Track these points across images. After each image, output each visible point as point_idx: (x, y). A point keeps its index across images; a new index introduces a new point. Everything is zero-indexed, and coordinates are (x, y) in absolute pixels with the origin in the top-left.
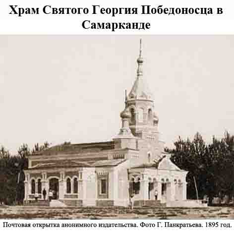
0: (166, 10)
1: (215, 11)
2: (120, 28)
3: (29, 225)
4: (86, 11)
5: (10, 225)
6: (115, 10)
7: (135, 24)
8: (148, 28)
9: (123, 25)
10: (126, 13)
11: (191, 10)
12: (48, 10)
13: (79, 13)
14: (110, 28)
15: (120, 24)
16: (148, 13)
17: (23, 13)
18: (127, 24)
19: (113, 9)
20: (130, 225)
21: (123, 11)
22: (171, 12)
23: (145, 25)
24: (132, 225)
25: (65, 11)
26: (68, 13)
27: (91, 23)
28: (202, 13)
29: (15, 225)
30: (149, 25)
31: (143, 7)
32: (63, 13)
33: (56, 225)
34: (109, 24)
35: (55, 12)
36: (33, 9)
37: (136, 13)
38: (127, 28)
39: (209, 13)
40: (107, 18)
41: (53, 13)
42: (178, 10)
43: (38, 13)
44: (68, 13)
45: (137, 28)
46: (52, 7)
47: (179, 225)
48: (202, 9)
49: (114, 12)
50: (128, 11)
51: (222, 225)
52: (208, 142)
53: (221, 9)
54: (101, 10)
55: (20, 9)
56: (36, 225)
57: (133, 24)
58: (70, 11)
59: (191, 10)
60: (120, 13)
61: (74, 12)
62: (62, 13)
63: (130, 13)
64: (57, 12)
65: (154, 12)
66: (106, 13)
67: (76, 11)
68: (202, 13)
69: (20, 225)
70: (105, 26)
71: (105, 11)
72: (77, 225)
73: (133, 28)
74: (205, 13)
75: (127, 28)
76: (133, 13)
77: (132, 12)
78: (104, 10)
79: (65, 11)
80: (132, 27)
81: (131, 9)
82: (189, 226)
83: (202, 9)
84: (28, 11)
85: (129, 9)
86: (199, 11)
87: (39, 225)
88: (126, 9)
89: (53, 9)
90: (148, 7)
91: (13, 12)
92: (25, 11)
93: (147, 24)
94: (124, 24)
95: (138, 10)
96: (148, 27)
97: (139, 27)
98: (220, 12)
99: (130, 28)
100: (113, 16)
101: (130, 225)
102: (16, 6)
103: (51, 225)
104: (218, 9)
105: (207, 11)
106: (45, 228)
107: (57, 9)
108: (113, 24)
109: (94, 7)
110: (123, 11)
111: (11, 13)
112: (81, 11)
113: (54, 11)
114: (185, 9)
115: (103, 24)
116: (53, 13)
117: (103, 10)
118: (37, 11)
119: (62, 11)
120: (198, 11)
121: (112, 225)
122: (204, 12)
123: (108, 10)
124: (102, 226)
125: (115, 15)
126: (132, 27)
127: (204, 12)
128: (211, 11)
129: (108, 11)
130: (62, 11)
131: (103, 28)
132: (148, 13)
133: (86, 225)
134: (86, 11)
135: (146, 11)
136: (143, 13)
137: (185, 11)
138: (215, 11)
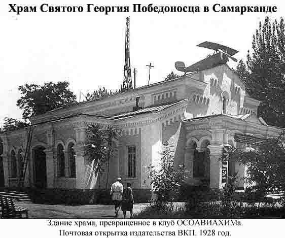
1: (202, 9)
2: (248, 11)
3: (91, 234)
5: (67, 234)
11: (180, 9)
12: (45, 8)
13: (74, 11)
14: (239, 11)
15: (248, 7)
16: (139, 11)
17: (22, 11)
18: (255, 8)
19: (106, 8)
21: (116, 9)
22: (161, 10)
23: (272, 8)
24: (170, 234)
25: (61, 9)
26: (64, 11)
27: (221, 6)
28: (189, 11)
29: (74, 234)
30: (276, 8)
31: (135, 5)
32: (59, 11)
35: (52, 10)
36: (229, 8)
37: (128, 11)
38: (255, 11)
39: (196, 11)
41: (50, 11)
43: (35, 11)
44: (64, 11)
45: (264, 11)
46: (49, 6)
47: (106, 234)
48: (189, 7)
53: (208, 8)
54: (95, 9)
55: (18, 7)
57: (261, 7)
58: (66, 9)
59: (180, 9)
63: (121, 11)
64: (53, 11)
65: (144, 10)
66: (99, 11)
67: (263, 9)
68: (189, 11)
69: (79, 233)
70: (234, 9)
73: (261, 11)
77: (123, 10)
78: (98, 8)
79: (61, 9)
80: (259, 10)
81: (123, 8)
82: (120, 234)
83: (189, 7)
84: (26, 10)
85: (121, 7)
86: (187, 9)
89: (50, 7)
90: (139, 5)
91: (12, 10)
92: (24, 9)
94: (252, 7)
95: (87, 10)
96: (275, 10)
97: (266, 11)
99: (258, 11)
100: (106, 14)
102: (15, 5)
103: (117, 234)
104: (205, 7)
105: (194, 9)
107: (53, 8)
108: (242, 7)
109: (89, 5)
110: (116, 9)
112: (76, 9)
115: (233, 8)
118: (81, 9)
119: (58, 9)
121: (146, 234)
122: (191, 10)
123: (102, 8)
124: (135, 234)
126: (259, 10)
127: (191, 10)
128: (198, 10)
130: (58, 9)
131: (233, 11)
132: (139, 11)
133: (158, 234)
135: (137, 9)
136: (135, 11)
137: (173, 9)
138: (202, 9)
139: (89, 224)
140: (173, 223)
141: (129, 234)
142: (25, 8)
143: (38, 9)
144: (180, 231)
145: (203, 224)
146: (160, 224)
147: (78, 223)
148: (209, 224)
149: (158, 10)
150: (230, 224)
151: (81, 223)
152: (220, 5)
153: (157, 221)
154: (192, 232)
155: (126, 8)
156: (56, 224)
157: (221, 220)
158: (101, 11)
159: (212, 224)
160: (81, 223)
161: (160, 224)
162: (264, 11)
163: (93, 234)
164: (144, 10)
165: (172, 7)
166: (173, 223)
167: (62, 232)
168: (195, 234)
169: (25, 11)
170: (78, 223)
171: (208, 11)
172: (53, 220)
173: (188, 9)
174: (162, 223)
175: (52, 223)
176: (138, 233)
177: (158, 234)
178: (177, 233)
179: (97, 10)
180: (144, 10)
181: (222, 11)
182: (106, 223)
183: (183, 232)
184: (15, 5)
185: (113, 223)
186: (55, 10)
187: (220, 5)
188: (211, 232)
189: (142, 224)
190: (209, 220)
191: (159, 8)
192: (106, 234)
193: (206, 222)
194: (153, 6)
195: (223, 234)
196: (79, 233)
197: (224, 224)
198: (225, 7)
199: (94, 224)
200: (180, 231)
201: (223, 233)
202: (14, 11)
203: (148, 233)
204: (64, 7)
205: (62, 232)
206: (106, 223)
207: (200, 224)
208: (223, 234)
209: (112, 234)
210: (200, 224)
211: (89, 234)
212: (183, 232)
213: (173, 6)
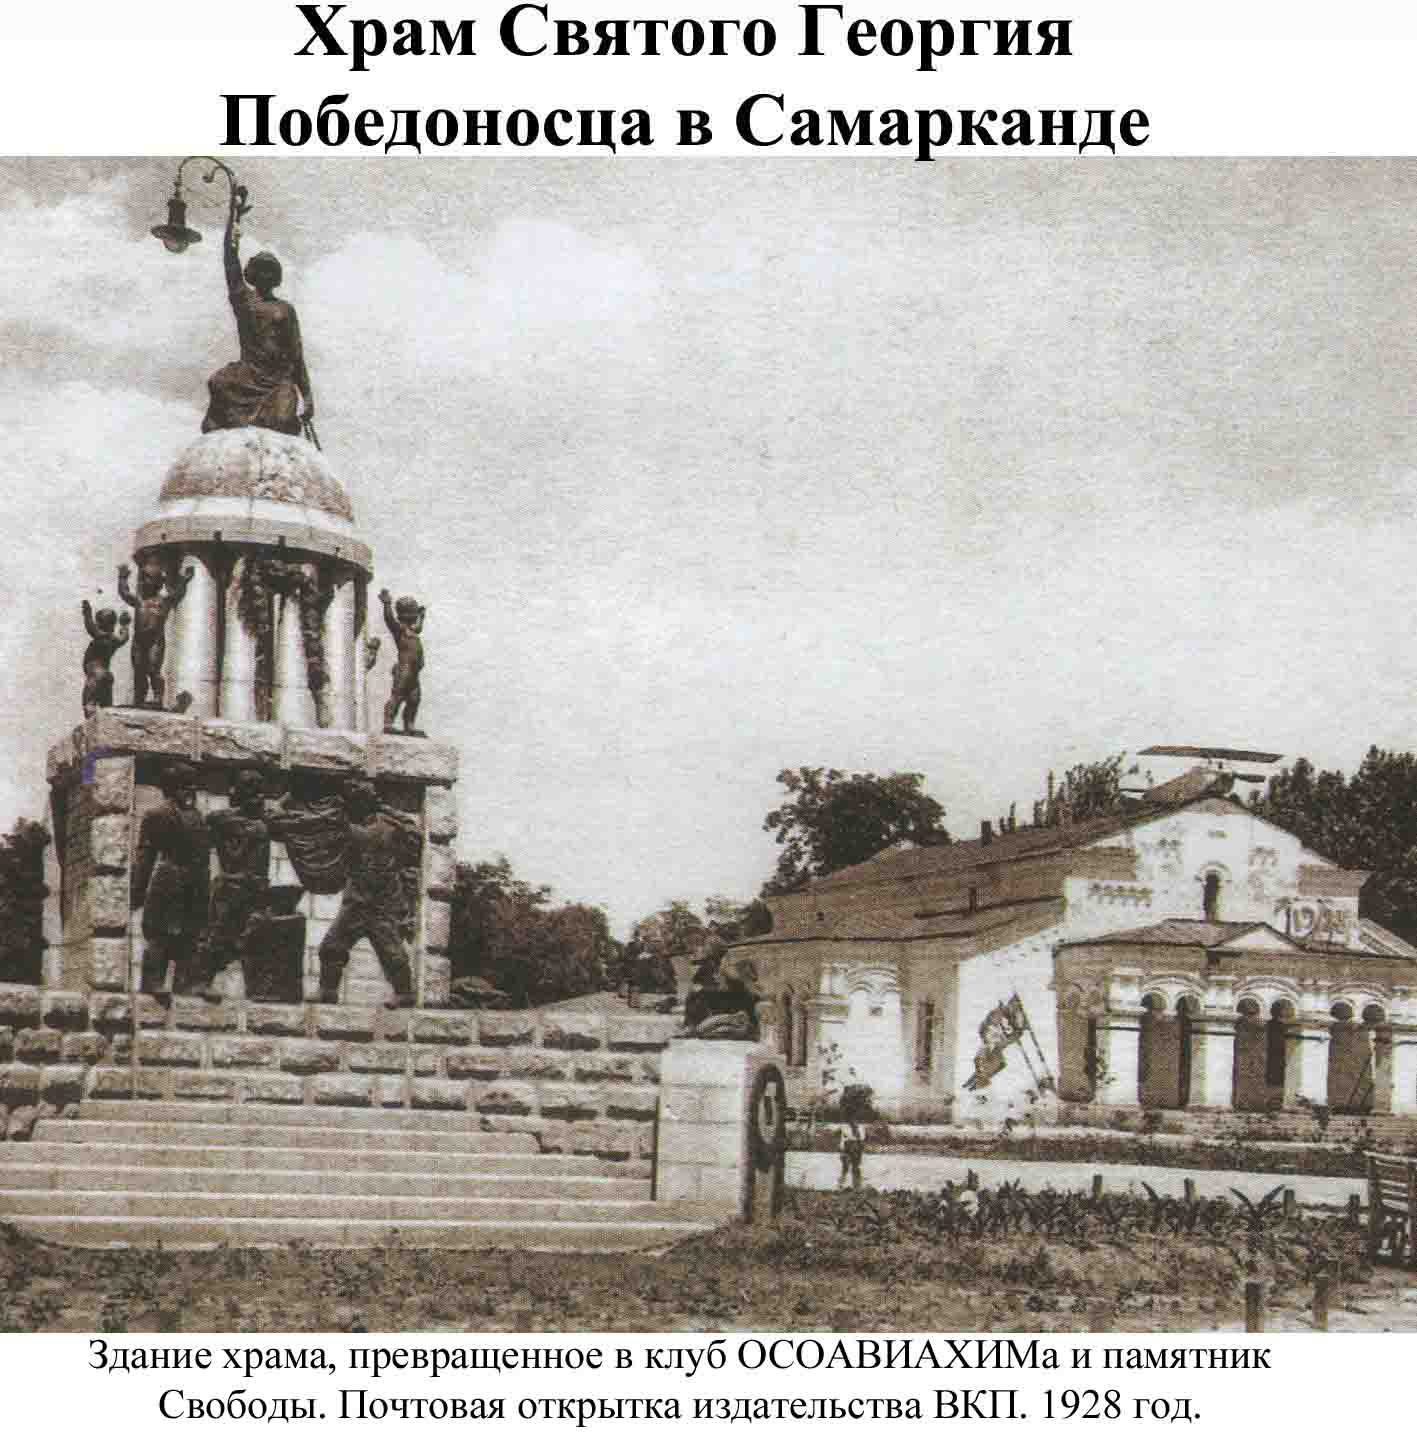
0: (370, 119)
1: (666, 129)
2: (967, 140)
3: (498, 1410)
4: (760, 38)
5: (378, 1409)
6: (937, 34)
7: (1058, 120)
8: (1130, 140)
9: (987, 124)
10: (1003, 49)
13: (718, 49)
14: (904, 139)
15: (967, 116)
18: (1007, 118)
19: (926, 27)
20: (882, 1409)
21: (985, 39)
22: (402, 136)
24: (894, 1408)
25: (636, 39)
26: (651, 48)
27: (791, 108)
29: (412, 1409)
30: (1144, 122)
32: (621, 50)
33: (661, 1408)
34: (1025, 117)
35: (573, 45)
37: (1064, 50)
38: (1008, 139)
39: (627, 139)
40: (891, 83)
41: (563, 49)
42: (442, 132)
43: (467, 50)
44: (651, 48)
45: (1068, 139)
46: (555, 14)
47: (574, 1408)
48: (586, 117)
49: (929, 42)
50: (1012, 38)
51: (1146, 1408)
52: (554, 904)
53: (704, 117)
54: (855, 26)
55: (359, 27)
56: (541, 1408)
57: (1047, 116)
58: (664, 38)
60: (969, 49)
61: (688, 45)
62: (613, 47)
63: (1023, 50)
64: (584, 46)
66: (880, 48)
69: (439, 1409)
70: (876, 128)
71: (877, 40)
72: (756, 1410)
74: (606, 139)
75: (1008, 139)
76: (1046, 50)
77: (1036, 42)
78: (871, 31)
79: (636, 39)
80: (1036, 131)
81: (1033, 30)
82: (641, 1409)
83: (586, 117)
85: (1023, 27)
86: (570, 130)
87: (554, 1409)
88: (1003, 26)
89: (563, 26)
90: (263, 103)
91: (319, 46)
92: (392, 38)
93: (1127, 116)
94: (992, 115)
96: (1137, 133)
98: (696, 135)
100: (926, 65)
101: (882, 1409)
102: (336, 8)
103: (627, 1410)
104: (685, 116)
105: (618, 128)
106: (594, 1423)
107: (582, 28)
108: (924, 117)
109: (811, 13)
110: (985, 39)
111: (304, 52)
112: (733, 38)
113: (569, 38)
114: (482, 120)
115: (864, 117)
116: (563, 49)
117: (862, 29)
120: (562, 129)
121: (773, 1409)
124: (716, 1409)
125: (935, 59)
126: (1036, 131)
129: (894, 37)
132: (262, 138)
133: (831, 1409)
134: (760, 38)
138: (666, 129)
139: (299, 1360)
140: (717, 1358)
141: (688, 1409)
142: (399, 29)
143: (487, 36)
144: (947, 1398)
145: (869, 1360)
146: (652, 1360)
147: (241, 1358)
148: (900, 1361)
149: (386, 131)
150: (1004, 1361)
151: (254, 1357)
152: (780, 101)
153: (638, 1343)
154: (1003, 1401)
155: (1054, 30)
156: (141, 1361)
157: (959, 1338)
158: (890, 51)
159: (913, 1362)
160: (254, 1357)
161: (652, 1360)
162: (1068, 139)
163: (510, 1409)
164: (296, 132)
165: (472, 116)
166: (717, 1358)
167: (353, 1401)
168: (1017, 1413)
169: (399, 49)
170: (241, 1358)
171: (707, 136)
172: (115, 1340)
173: (573, 130)
174: (663, 1359)
175: (109, 1353)
176: (732, 1408)
177: (831, 1409)
178: (929, 1406)
179: (865, 43)
180: (296, 132)
181: (797, 139)
182: (382, 1357)
183: (960, 1403)
184: (336, 8)
185: (419, 1358)
186: (595, 42)
187: (780, 101)
188: (1103, 1403)
189: (561, 1359)
190: (898, 1339)
191: (809, 1404)
192: (574, 1408)
193: (883, 1353)
194: (351, 110)
195: (1161, 1409)
196: (439, 1409)
197: (973, 1360)
198: (814, 117)
199: (321, 1361)
200: (947, 1398)
201: (1160, 1409)
202: (333, 48)
203: (786, 1408)
204: (651, 27)
205: (353, 1401)
206: (382, 1357)
207: (854, 1360)
208: (1161, 1409)
209: (603, 1410)
210: (854, 1360)
211: (488, 1410)
212: (960, 1403)
213: (482, 105)
